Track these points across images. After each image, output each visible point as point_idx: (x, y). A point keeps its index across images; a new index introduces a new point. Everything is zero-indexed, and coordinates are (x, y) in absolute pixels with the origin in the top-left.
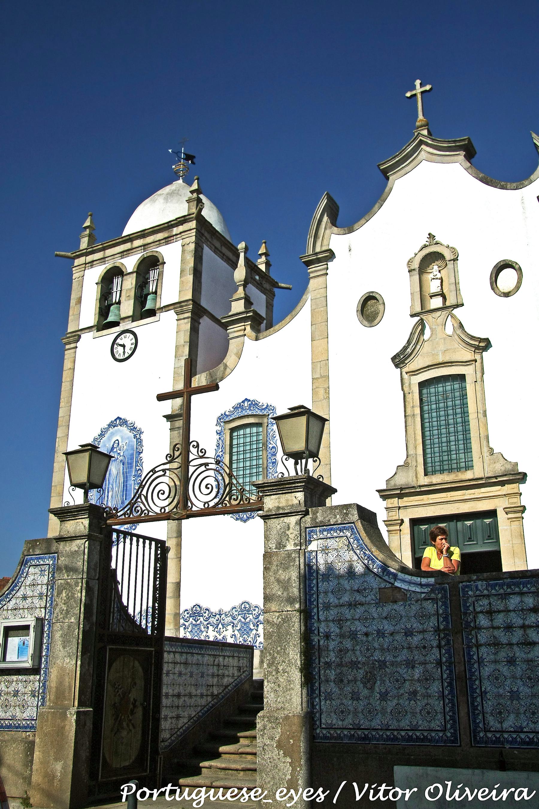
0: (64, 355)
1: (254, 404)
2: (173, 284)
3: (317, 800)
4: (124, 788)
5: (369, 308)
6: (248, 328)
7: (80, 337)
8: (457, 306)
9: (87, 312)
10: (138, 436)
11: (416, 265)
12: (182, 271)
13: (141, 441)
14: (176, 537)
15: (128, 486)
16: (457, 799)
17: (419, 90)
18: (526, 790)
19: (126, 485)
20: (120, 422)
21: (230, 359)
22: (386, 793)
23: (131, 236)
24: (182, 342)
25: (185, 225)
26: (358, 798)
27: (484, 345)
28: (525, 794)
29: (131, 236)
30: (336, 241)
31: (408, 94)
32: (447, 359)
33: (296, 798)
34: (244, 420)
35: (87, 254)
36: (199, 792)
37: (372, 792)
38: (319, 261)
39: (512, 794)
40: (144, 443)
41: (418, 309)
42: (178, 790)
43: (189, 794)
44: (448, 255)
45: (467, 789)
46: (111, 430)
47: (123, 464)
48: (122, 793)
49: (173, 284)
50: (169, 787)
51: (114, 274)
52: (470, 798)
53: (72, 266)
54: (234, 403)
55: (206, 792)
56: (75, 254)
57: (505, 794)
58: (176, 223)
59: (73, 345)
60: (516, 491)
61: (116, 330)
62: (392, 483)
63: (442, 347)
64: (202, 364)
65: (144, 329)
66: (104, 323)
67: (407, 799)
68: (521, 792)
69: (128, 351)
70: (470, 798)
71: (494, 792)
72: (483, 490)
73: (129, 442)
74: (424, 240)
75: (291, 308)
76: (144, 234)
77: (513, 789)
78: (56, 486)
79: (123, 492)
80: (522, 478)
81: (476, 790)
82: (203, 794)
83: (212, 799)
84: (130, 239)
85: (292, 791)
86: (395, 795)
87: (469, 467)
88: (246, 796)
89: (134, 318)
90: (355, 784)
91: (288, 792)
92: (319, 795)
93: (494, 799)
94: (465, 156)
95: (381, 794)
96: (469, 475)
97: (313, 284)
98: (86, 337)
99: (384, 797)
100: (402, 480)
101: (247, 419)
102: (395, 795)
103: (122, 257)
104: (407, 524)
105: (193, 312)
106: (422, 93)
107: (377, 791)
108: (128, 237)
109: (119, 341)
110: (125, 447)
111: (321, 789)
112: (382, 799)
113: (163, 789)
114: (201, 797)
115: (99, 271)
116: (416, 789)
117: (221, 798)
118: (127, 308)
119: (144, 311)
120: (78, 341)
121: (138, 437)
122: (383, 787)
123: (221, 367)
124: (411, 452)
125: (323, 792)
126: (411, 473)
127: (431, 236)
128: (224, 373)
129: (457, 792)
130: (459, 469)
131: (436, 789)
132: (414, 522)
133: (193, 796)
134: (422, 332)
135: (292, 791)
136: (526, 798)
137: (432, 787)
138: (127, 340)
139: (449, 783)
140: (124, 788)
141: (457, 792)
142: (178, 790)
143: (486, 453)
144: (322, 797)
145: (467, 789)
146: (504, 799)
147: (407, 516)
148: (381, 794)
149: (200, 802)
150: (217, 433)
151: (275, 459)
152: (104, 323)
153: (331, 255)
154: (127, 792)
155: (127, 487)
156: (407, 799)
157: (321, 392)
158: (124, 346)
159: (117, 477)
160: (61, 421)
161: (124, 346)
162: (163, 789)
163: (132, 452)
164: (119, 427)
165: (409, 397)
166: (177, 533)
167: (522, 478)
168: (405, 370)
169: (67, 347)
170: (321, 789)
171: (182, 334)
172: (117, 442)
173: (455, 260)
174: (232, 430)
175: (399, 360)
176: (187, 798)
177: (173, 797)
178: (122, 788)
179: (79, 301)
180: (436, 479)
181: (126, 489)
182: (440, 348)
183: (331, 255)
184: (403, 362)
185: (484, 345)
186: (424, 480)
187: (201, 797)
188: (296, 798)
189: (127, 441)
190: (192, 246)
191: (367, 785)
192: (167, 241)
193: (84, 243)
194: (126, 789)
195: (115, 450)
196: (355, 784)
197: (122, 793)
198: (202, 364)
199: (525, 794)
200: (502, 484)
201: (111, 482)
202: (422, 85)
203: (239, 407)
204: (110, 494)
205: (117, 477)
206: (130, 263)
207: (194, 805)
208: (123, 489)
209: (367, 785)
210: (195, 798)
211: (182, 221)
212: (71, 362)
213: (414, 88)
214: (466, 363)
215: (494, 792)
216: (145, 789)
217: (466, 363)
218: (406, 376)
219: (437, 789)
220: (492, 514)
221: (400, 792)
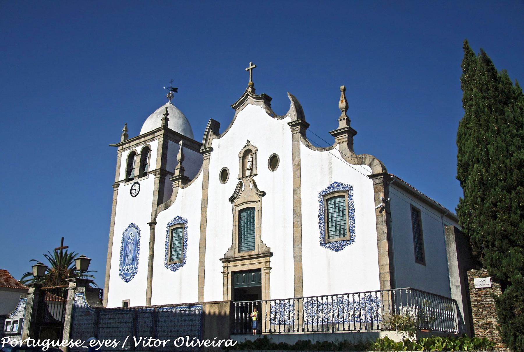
0: (113, 193)
2: (154, 162)
3: (113, 346)
5: (224, 175)
6: (180, 183)
7: (119, 185)
8: (255, 175)
9: (122, 174)
11: (242, 155)
16: (192, 346)
17: (251, 67)
18: (231, 341)
21: (173, 198)
22: (152, 342)
24: (156, 189)
26: (136, 345)
27: (263, 194)
28: (231, 343)
30: (214, 142)
31: (246, 69)
32: (249, 200)
33: (101, 345)
35: (123, 145)
36: (46, 342)
37: (144, 341)
38: (207, 152)
39: (223, 343)
41: (241, 176)
43: (40, 344)
44: (254, 151)
45: (198, 340)
46: (129, 229)
49: (154, 162)
51: (133, 155)
52: (200, 345)
53: (117, 151)
54: (173, 218)
57: (219, 343)
59: (117, 189)
60: (268, 260)
61: (133, 182)
62: (226, 255)
63: (248, 194)
64: (163, 198)
65: (143, 181)
66: (128, 179)
67: (164, 346)
68: (229, 342)
69: (137, 192)
70: (200, 345)
71: (214, 342)
72: (258, 259)
74: (245, 143)
75: (195, 174)
77: (224, 340)
80: (271, 255)
81: (203, 341)
82: (48, 343)
83: (53, 346)
85: (99, 341)
86: (157, 343)
87: (253, 249)
88: (73, 344)
89: (140, 176)
90: (134, 337)
91: (97, 342)
92: (114, 344)
93: (213, 346)
94: (264, 102)
95: (149, 343)
96: (253, 253)
97: (205, 162)
98: (122, 185)
99: (151, 344)
100: (230, 254)
102: (157, 343)
103: (136, 147)
104: (230, 274)
105: (161, 174)
106: (252, 69)
107: (147, 342)
109: (134, 188)
111: (115, 340)
112: (150, 346)
113: (25, 340)
115: (125, 154)
116: (169, 340)
118: (136, 171)
119: (143, 174)
120: (118, 187)
122: (151, 339)
123: (170, 201)
124: (234, 242)
125: (116, 342)
126: (233, 252)
127: (248, 141)
129: (193, 342)
130: (250, 250)
131: (181, 341)
132: (234, 273)
133: (43, 344)
134: (241, 187)
135: (99, 341)
136: (232, 345)
137: (178, 339)
138: (136, 187)
139: (188, 337)
141: (193, 342)
142: (34, 341)
143: (260, 243)
144: (116, 344)
145: (198, 340)
146: (219, 346)
147: (230, 270)
148: (149, 343)
152: (128, 179)
153: (211, 149)
156: (164, 346)
157: (204, 213)
158: (135, 190)
160: (112, 224)
161: (135, 190)
162: (25, 340)
165: (235, 216)
167: (271, 255)
168: (234, 204)
169: (115, 189)
170: (115, 340)
171: (156, 185)
173: (256, 153)
174: (173, 230)
175: (232, 200)
176: (39, 346)
179: (120, 168)
180: (241, 254)
182: (248, 194)
183: (211, 149)
184: (233, 201)
185: (263, 194)
186: (237, 255)
188: (101, 345)
190: (162, 142)
191: (141, 338)
192: (153, 139)
193: (122, 140)
194: (4, 340)
196: (134, 337)
198: (163, 198)
199: (231, 343)
200: (264, 257)
202: (252, 65)
203: (175, 220)
206: (139, 150)
207: (43, 349)
209: (141, 338)
210: (44, 345)
211: (158, 130)
213: (249, 66)
214: (256, 202)
215: (214, 342)
216: (158, 340)
217: (256, 202)
218: (234, 207)
219: (181, 341)
220: (260, 270)
221: (160, 342)
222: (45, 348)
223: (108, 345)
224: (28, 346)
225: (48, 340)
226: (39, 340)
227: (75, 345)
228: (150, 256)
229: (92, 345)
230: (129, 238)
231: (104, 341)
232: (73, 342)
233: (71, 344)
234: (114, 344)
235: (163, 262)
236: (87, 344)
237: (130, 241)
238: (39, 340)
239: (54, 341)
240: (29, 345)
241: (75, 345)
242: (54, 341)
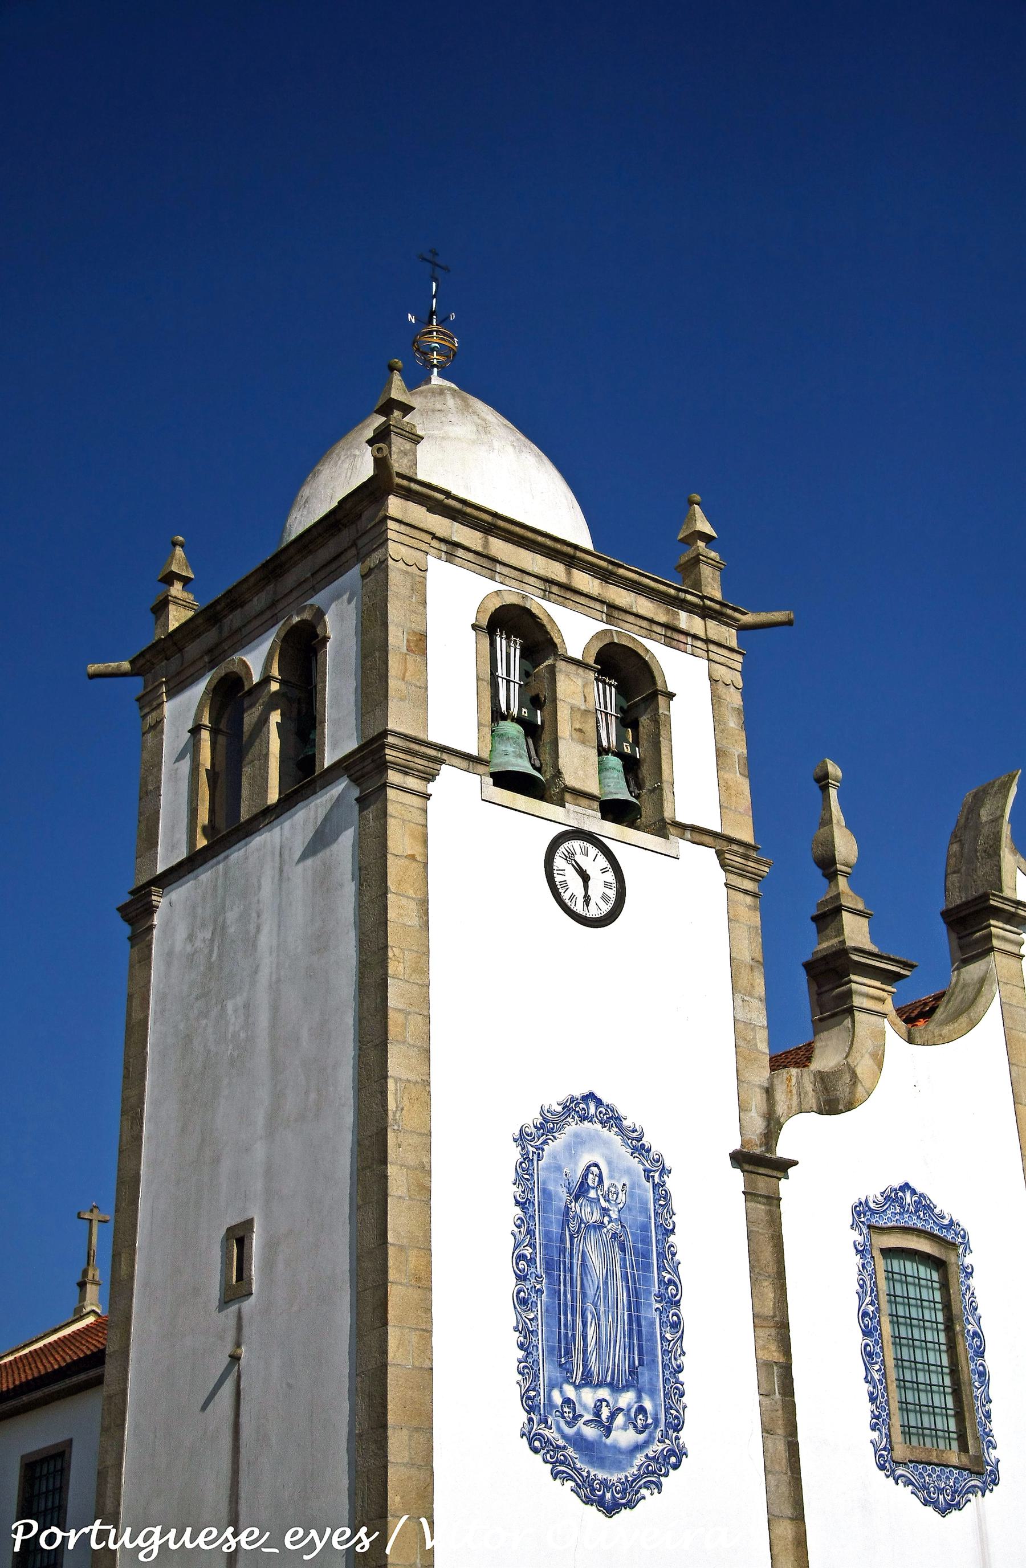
1: (924, 1205)
3: (225, 1549)
4: (17, 1528)
10: (657, 1175)
12: (479, 725)
13: (667, 1197)
14: (790, 1518)
15: (643, 1323)
19: (638, 1319)
20: (588, 1107)
23: (579, 554)
25: (711, 624)
29: (579, 554)
34: (909, 1237)
36: (150, 1534)
40: (676, 1205)
42: (113, 1532)
46: (573, 1127)
47: (622, 1249)
48: (13, 1536)
50: (97, 1526)
55: (162, 1535)
56: (405, 483)
58: (695, 605)
73: (633, 1187)
76: (612, 573)
78: (401, 1248)
79: (631, 1337)
82: (156, 1537)
83: (172, 1546)
84: (573, 557)
88: (233, 1542)
92: (360, 1540)
101: (915, 1238)
108: (570, 550)
110: (622, 1197)
111: (364, 1529)
113: (86, 1530)
114: (152, 1544)
117: (189, 1546)
121: (657, 1180)
125: (368, 1535)
128: (852, 1093)
133: (140, 1541)
135: (313, 1533)
140: (17, 1528)
142: (113, 1532)
144: (366, 1542)
149: (151, 1552)
150: (858, 1251)
151: (982, 1365)
154: (24, 1534)
155: (639, 1325)
159: (606, 1283)
162: (86, 1530)
163: (641, 1219)
164: (599, 1126)
166: (795, 1508)
170: (364, 1529)
171: (743, 932)
172: (594, 1169)
177: (104, 1543)
178: (14, 1527)
179: (419, 643)
181: (640, 1332)
187: (152, 1544)
188: (319, 1546)
189: (625, 1180)
194: (21, 1529)
195: (592, 1194)
197: (13, 1536)
201: (591, 1292)
204: (591, 1331)
205: (606, 1283)
208: (631, 1330)
210: (142, 1545)
212: (413, 836)
216: (54, 1529)
221: (60, 1534)
222: (148, 1555)
223: (293, 1543)
224: (94, 1546)
225: (157, 1530)
226: (189, 1530)
227: (238, 1543)
228: (764, 1366)
229: (293, 1543)
230: (581, 1191)
231: (328, 1530)
232: (235, 1535)
233: (227, 1540)
234: (360, 1540)
235: (862, 1438)
236: (277, 1540)
237: (590, 1214)
238: (189, 1530)
239: (173, 1531)
240: (98, 1543)
241: (238, 1543)
242: (173, 1531)
